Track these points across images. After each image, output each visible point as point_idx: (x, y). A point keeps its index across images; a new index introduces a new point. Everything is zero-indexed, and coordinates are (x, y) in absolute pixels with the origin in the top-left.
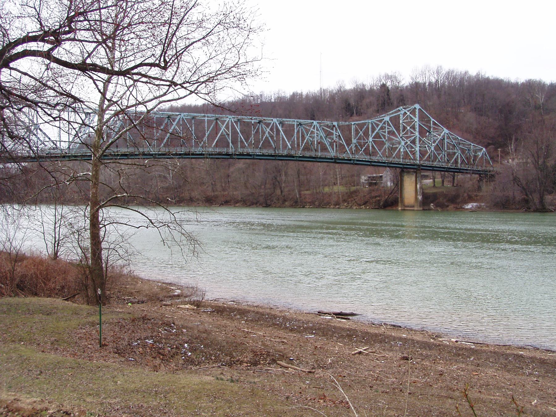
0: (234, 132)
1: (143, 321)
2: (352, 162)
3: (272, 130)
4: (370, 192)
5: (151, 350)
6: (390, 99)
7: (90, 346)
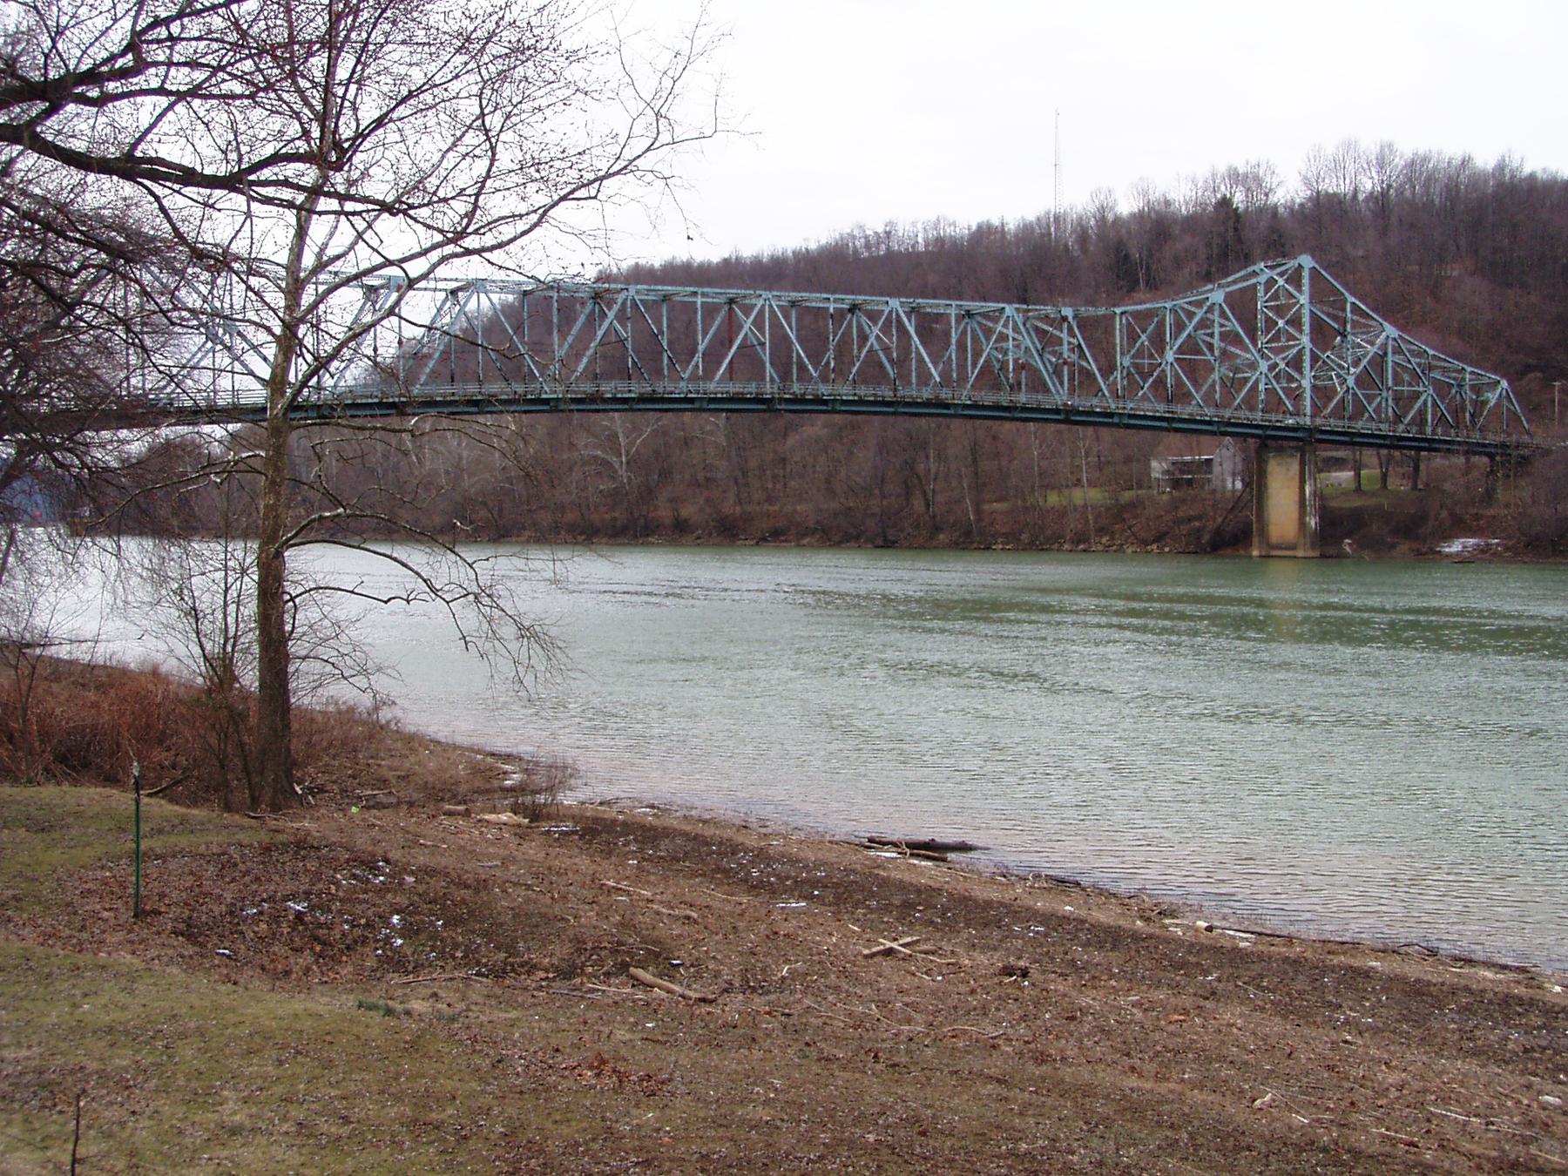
0: (780, 340)
1: (296, 853)
2: (1116, 420)
3: (886, 329)
4: (1175, 504)
5: (294, 929)
6: (1240, 241)
7: (106, 914)
